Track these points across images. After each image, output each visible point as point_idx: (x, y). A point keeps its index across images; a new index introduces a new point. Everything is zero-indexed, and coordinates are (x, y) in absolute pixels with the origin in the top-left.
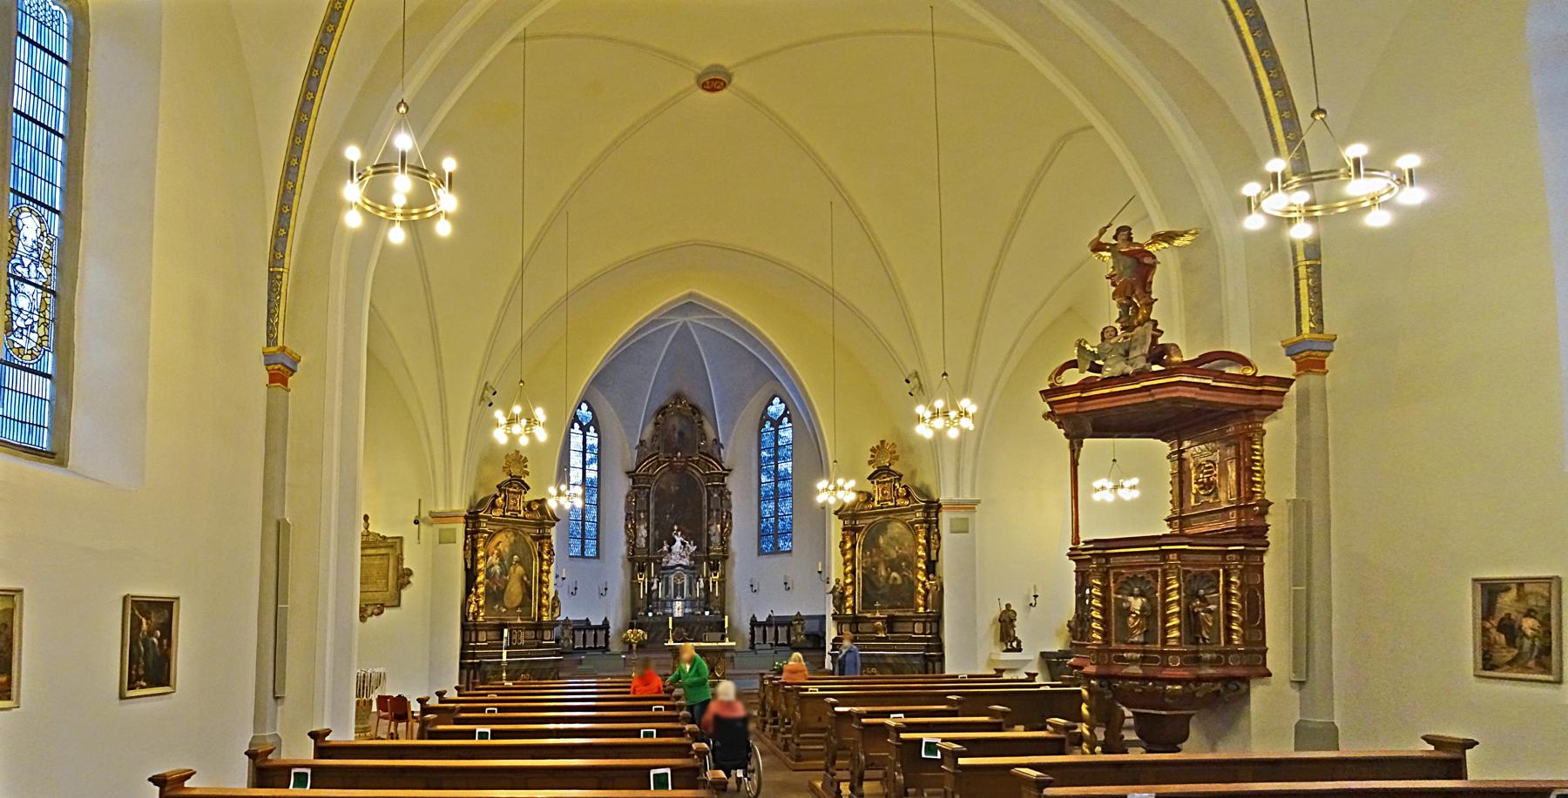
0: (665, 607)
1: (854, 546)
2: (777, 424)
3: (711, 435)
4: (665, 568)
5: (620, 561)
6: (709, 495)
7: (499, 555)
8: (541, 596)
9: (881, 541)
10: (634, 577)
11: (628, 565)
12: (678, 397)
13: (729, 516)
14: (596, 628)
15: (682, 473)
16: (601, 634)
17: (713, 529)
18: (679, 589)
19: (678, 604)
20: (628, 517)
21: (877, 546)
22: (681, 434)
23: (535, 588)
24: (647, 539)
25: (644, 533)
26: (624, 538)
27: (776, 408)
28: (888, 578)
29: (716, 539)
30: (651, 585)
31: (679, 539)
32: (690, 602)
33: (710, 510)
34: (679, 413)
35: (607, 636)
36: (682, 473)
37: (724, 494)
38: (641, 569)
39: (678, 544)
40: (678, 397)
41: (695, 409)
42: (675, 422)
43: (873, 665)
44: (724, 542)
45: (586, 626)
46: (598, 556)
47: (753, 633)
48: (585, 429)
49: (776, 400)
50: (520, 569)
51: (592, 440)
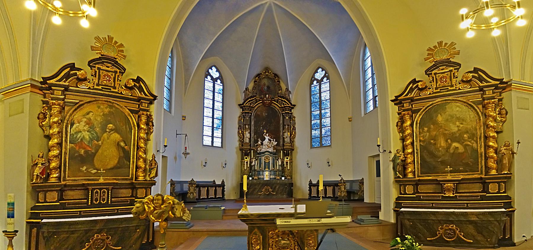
0: (259, 174)
1: (412, 125)
2: (320, 82)
3: (284, 87)
4: (258, 154)
5: (235, 150)
6: (284, 118)
7: (89, 123)
8: (138, 158)
9: (440, 118)
10: (242, 159)
11: (240, 152)
12: (267, 69)
13: (294, 129)
14: (219, 186)
15: (269, 107)
16: (219, 190)
17: (286, 134)
18: (267, 165)
19: (267, 173)
20: (240, 128)
21: (435, 123)
22: (268, 87)
23: (133, 153)
24: (250, 139)
25: (248, 135)
26: (237, 138)
27: (319, 75)
28: (448, 148)
29: (287, 140)
30: (251, 162)
31: (267, 138)
32: (274, 172)
33: (284, 125)
34: (267, 77)
35: (223, 191)
36: (269, 107)
37: (292, 118)
38: (247, 154)
39: (267, 140)
40: (267, 69)
41: (276, 75)
42: (265, 81)
43: (452, 222)
44: (292, 142)
45: (213, 185)
46: (222, 147)
47: (310, 190)
48: (214, 80)
49: (320, 70)
50: (116, 136)
51: (219, 87)
